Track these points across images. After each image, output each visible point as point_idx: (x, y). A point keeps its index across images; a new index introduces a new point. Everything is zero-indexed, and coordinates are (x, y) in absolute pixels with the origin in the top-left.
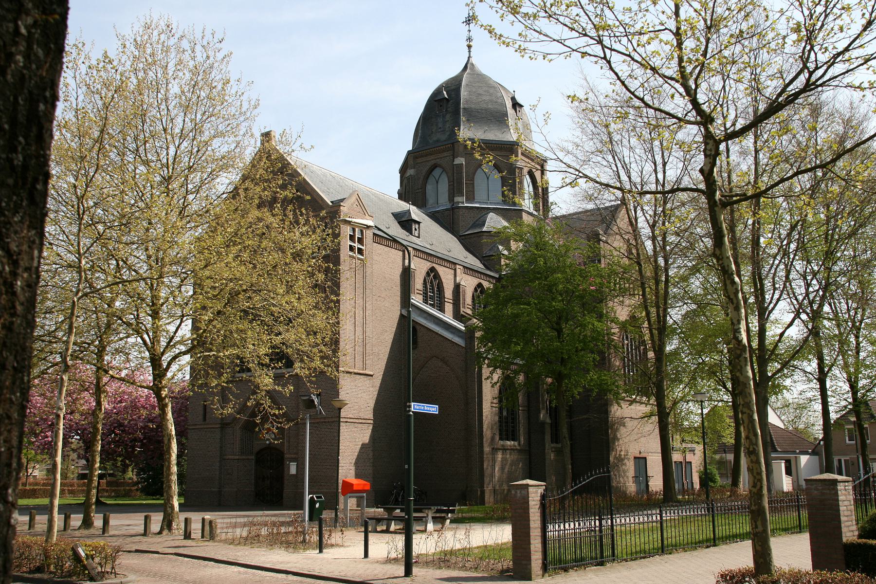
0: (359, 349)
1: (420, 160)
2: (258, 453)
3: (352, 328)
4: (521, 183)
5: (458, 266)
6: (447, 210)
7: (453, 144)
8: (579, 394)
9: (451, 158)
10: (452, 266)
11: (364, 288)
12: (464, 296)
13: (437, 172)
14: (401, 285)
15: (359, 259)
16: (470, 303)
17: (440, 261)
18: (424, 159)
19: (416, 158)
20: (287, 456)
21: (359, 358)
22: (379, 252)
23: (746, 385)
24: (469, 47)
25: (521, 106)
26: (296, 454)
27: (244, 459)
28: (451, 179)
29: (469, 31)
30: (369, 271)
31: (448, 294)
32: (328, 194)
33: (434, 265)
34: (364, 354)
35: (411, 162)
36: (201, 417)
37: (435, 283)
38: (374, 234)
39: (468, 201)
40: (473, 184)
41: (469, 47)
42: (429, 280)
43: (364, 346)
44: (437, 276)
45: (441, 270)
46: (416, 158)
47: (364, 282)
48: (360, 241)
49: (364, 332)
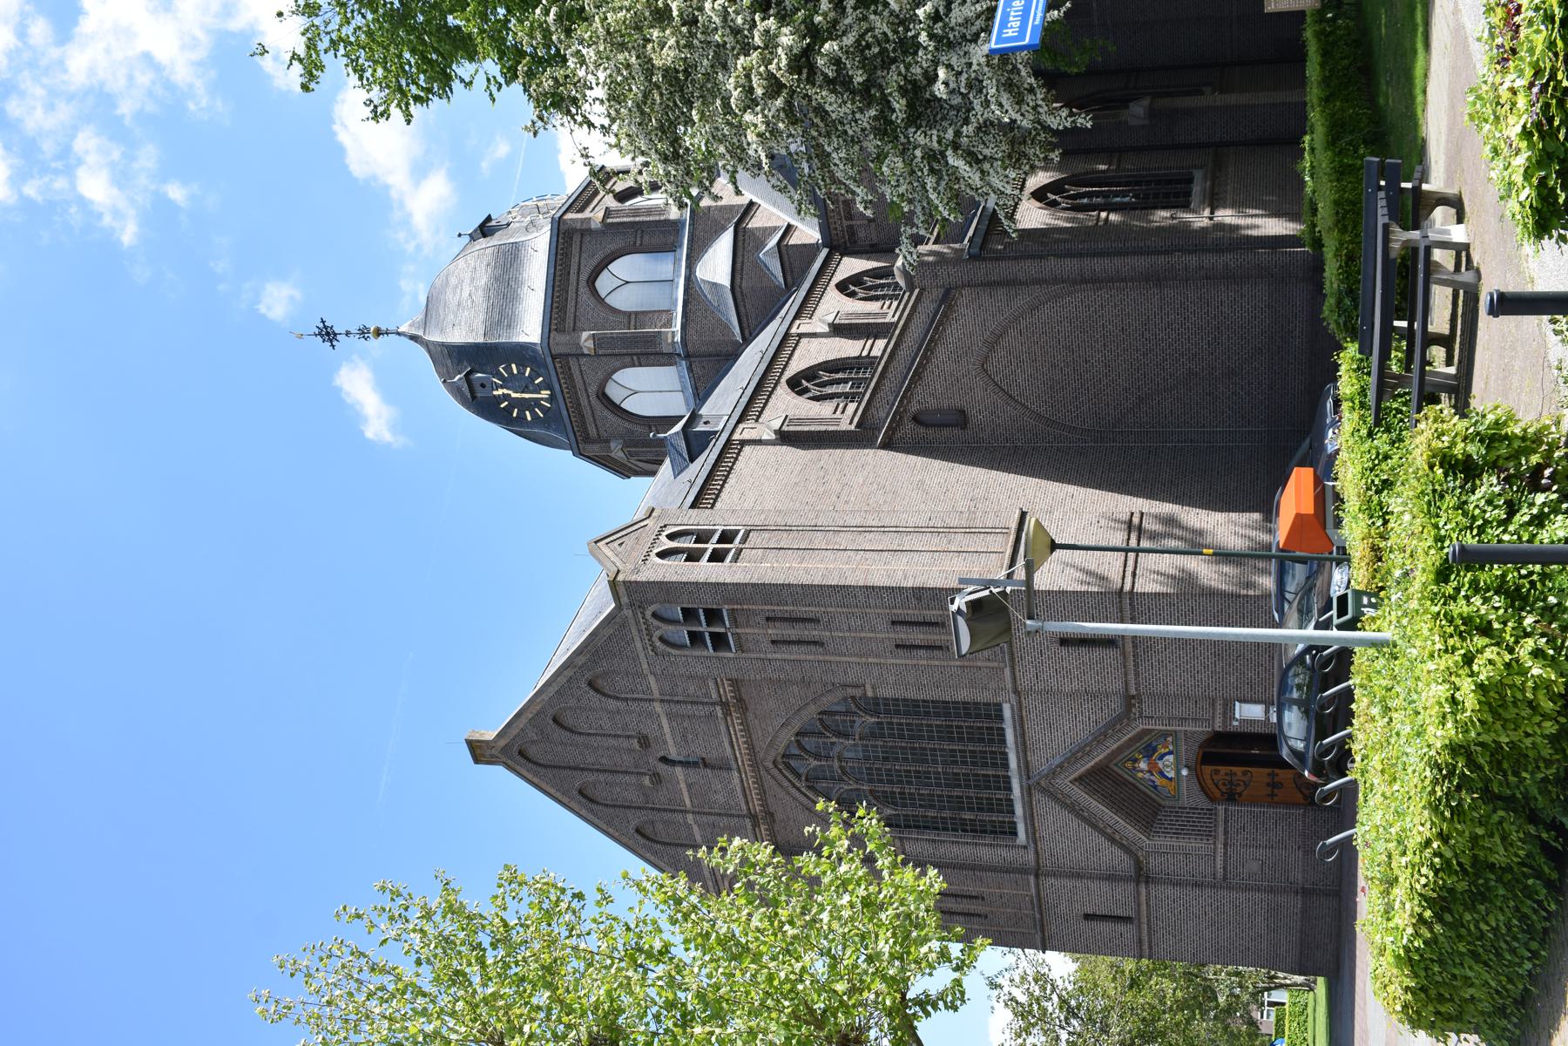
0: (960, 542)
1: (592, 431)
2: (1212, 799)
3: (904, 558)
4: (649, 211)
5: (794, 330)
6: (690, 369)
7: (554, 357)
8: (1455, 479)
9: (583, 361)
10: (792, 342)
11: (815, 528)
12: (858, 315)
13: (613, 391)
14: (819, 447)
15: (744, 540)
16: (879, 304)
17: (778, 367)
18: (589, 419)
19: (587, 439)
20: (1218, 727)
21: (978, 543)
22: (736, 495)
23: (1335, 88)
24: (378, 333)
25: (489, 219)
26: (1213, 703)
27: (1226, 833)
28: (628, 359)
29: (348, 333)
30: (773, 519)
31: (850, 348)
32: (606, 606)
33: (784, 380)
34: (969, 531)
35: (595, 449)
36: (1121, 928)
37: (825, 376)
38: (693, 506)
39: (669, 323)
40: (636, 313)
41: (378, 333)
42: (815, 391)
43: (949, 530)
44: (810, 374)
45: (797, 365)
46: (587, 439)
47: (801, 529)
48: (703, 537)
49: (918, 530)
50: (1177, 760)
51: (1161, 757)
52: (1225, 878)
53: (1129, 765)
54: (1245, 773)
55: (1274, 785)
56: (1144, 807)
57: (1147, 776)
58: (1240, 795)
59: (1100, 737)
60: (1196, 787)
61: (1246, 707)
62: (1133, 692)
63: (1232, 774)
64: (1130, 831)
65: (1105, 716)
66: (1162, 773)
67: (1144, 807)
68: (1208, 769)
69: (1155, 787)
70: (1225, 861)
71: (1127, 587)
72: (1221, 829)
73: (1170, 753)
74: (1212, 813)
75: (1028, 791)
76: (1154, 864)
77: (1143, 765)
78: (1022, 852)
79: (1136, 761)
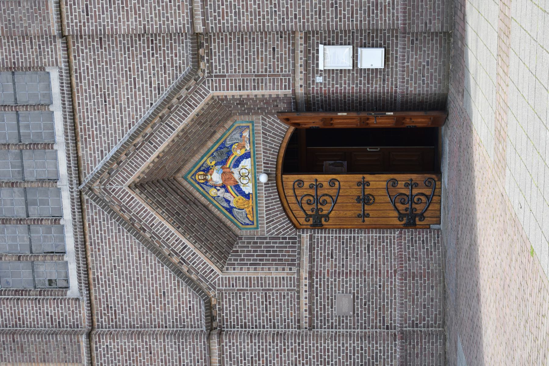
27: (311, 260)
50: (255, 165)
51: (236, 164)
52: (311, 327)
53: (200, 177)
54: (332, 182)
55: (366, 200)
56: (218, 236)
57: (221, 193)
58: (327, 217)
59: (166, 108)
60: (277, 206)
61: (330, 49)
62: (200, 28)
63: (317, 186)
64: (201, 259)
65: (168, 81)
66: (237, 187)
67: (218, 236)
68: (291, 179)
69: (230, 210)
70: (311, 298)
71: (215, 340)
72: (305, 258)
73: (247, 156)
74: (295, 241)
75: (80, 205)
76: (228, 309)
77: (216, 177)
78: (73, 306)
79: (207, 170)
